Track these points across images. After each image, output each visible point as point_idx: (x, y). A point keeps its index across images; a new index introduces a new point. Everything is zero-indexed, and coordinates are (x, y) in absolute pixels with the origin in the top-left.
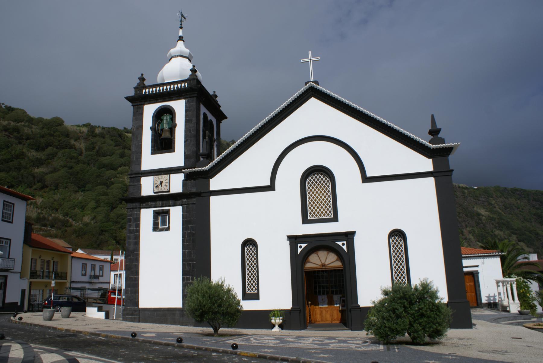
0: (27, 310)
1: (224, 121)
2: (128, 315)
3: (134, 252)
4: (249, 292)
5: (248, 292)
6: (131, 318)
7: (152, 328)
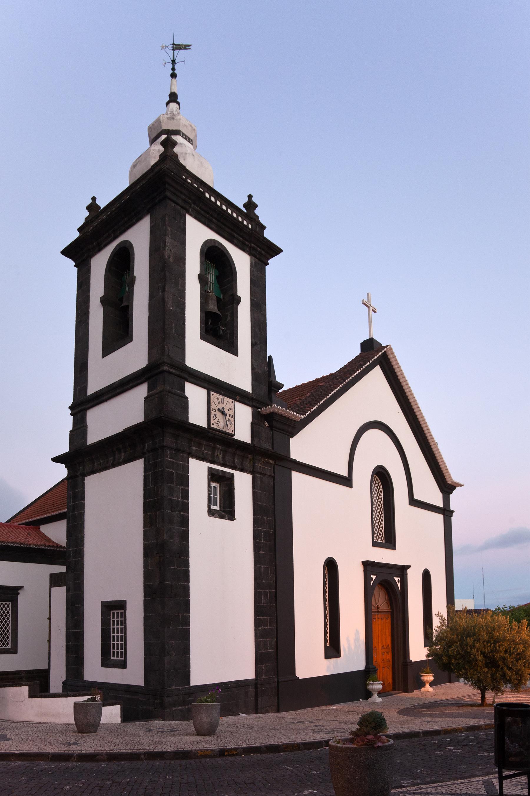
0: (60, 690)
2: (175, 707)
3: (180, 557)
6: (181, 710)
7: (382, 636)
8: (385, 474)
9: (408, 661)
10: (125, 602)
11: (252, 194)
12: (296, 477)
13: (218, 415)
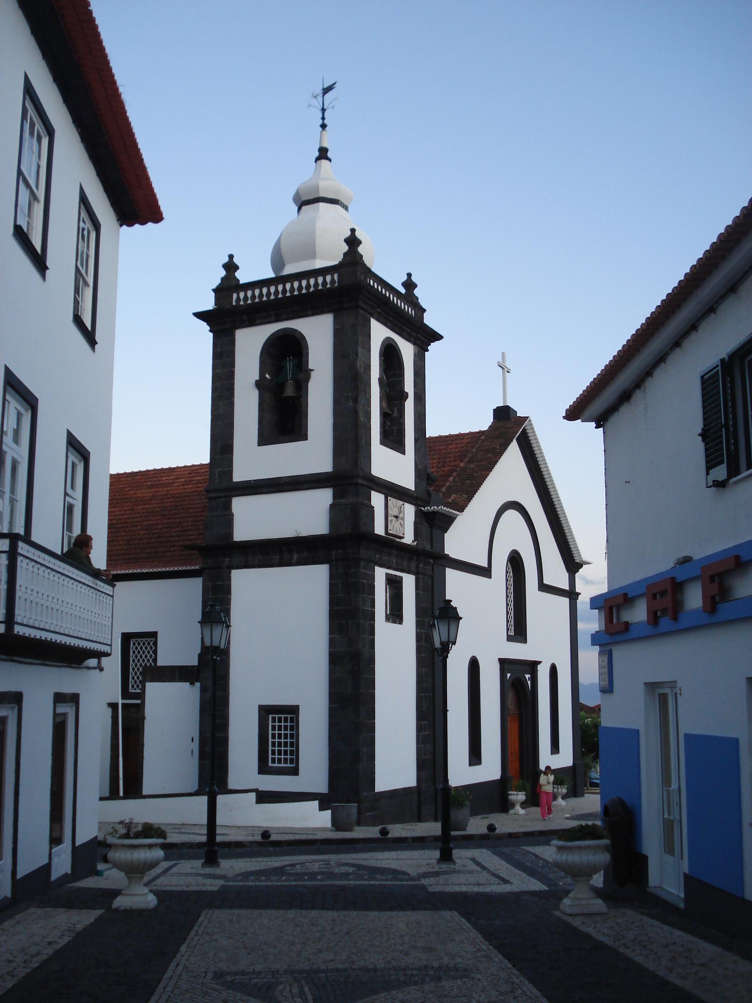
1: (433, 347)
4: (133, 691)
5: (509, 634)
8: (519, 559)
9: (539, 770)
10: (298, 707)
11: (411, 273)
12: (450, 574)
13: (393, 520)
